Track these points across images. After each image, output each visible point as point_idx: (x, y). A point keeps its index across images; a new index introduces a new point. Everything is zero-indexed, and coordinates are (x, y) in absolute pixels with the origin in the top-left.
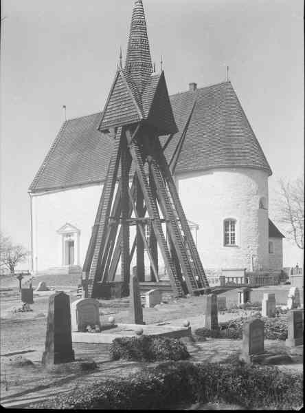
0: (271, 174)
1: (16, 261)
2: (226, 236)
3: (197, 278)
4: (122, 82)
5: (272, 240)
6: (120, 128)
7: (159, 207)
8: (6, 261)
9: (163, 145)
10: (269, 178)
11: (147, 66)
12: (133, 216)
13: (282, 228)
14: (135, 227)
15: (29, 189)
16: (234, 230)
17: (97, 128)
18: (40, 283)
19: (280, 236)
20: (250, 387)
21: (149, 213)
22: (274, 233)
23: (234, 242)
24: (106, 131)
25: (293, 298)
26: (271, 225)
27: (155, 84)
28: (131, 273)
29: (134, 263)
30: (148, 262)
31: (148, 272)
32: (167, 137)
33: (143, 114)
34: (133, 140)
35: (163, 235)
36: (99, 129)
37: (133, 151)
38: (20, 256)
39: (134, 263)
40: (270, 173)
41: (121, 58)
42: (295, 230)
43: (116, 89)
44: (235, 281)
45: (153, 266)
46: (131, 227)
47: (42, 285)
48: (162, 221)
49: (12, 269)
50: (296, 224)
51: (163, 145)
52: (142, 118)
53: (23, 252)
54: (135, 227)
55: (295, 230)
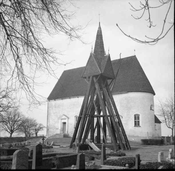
0: (155, 94)
1: (38, 130)
2: (135, 122)
3: (118, 142)
4: (93, 58)
5: (156, 124)
6: (91, 77)
7: (107, 109)
8: (34, 130)
9: (109, 84)
10: (154, 96)
11: (103, 51)
12: (96, 114)
13: (161, 119)
14: (96, 118)
15: (47, 99)
16: (139, 119)
17: (81, 76)
18: (52, 142)
19: (160, 122)
20: (161, 12)
21: (103, 112)
22: (157, 121)
23: (139, 125)
24: (85, 78)
25: (171, 154)
26: (156, 117)
27: (106, 60)
28: (95, 138)
29: (96, 134)
30: (102, 134)
31: (102, 138)
32: (111, 80)
33: (101, 71)
34: (97, 82)
35: (109, 121)
36: (82, 77)
37: (97, 86)
38: (40, 128)
39: (96, 134)
40: (154, 94)
41: (92, 49)
42: (166, 120)
43: (90, 61)
44: (108, 149)
45: (104, 137)
46: (95, 118)
47: (53, 143)
48: (109, 116)
49: (36, 134)
50: (166, 117)
51: (109, 84)
52: (100, 73)
53: (42, 126)
54: (96, 118)
55: (166, 120)
